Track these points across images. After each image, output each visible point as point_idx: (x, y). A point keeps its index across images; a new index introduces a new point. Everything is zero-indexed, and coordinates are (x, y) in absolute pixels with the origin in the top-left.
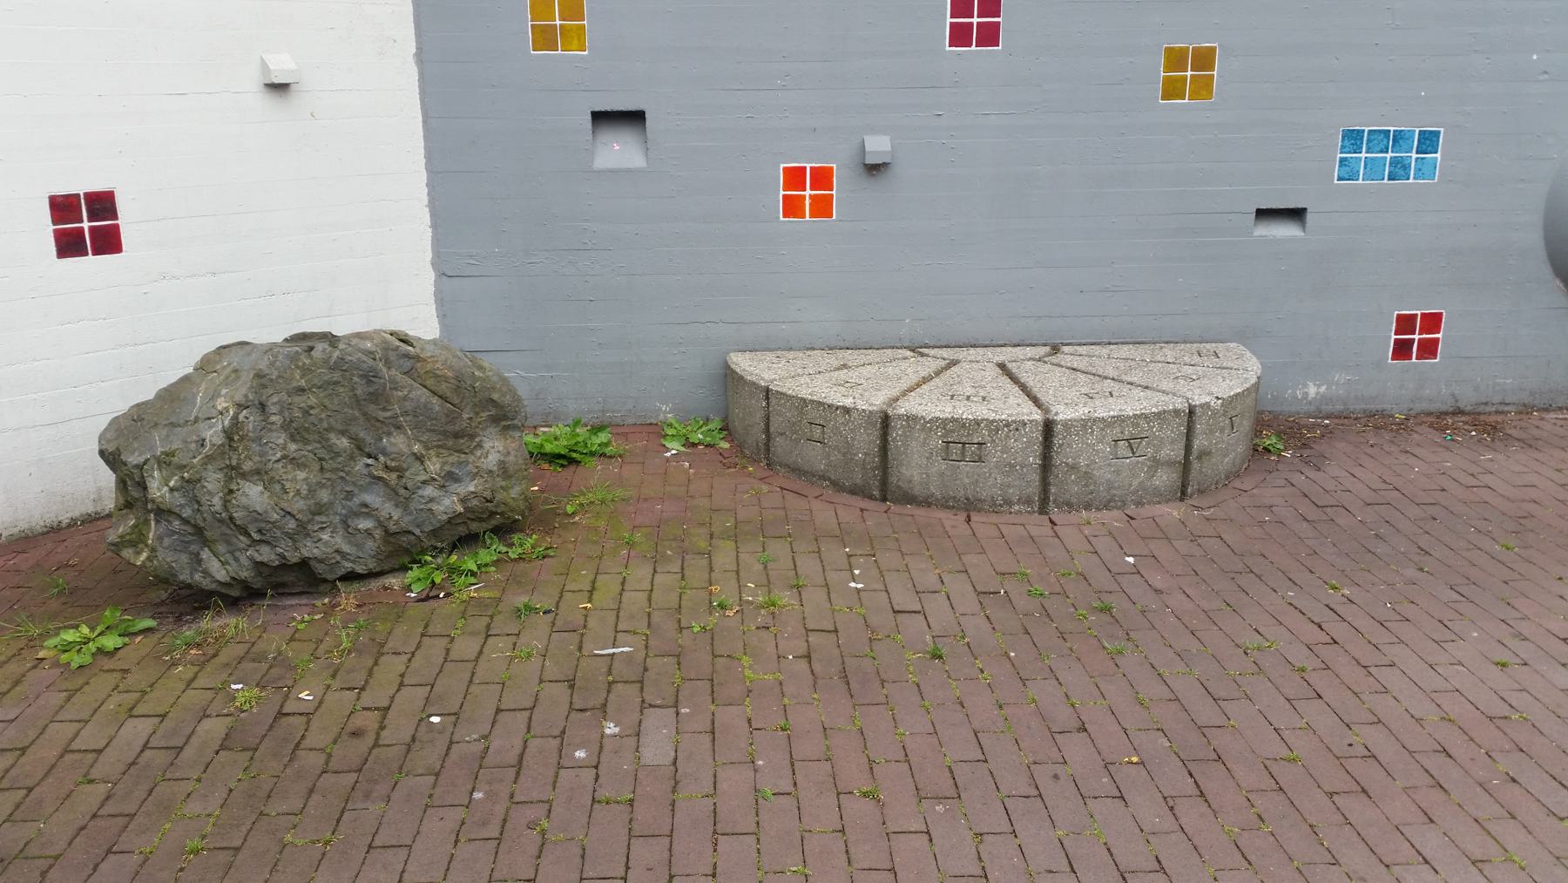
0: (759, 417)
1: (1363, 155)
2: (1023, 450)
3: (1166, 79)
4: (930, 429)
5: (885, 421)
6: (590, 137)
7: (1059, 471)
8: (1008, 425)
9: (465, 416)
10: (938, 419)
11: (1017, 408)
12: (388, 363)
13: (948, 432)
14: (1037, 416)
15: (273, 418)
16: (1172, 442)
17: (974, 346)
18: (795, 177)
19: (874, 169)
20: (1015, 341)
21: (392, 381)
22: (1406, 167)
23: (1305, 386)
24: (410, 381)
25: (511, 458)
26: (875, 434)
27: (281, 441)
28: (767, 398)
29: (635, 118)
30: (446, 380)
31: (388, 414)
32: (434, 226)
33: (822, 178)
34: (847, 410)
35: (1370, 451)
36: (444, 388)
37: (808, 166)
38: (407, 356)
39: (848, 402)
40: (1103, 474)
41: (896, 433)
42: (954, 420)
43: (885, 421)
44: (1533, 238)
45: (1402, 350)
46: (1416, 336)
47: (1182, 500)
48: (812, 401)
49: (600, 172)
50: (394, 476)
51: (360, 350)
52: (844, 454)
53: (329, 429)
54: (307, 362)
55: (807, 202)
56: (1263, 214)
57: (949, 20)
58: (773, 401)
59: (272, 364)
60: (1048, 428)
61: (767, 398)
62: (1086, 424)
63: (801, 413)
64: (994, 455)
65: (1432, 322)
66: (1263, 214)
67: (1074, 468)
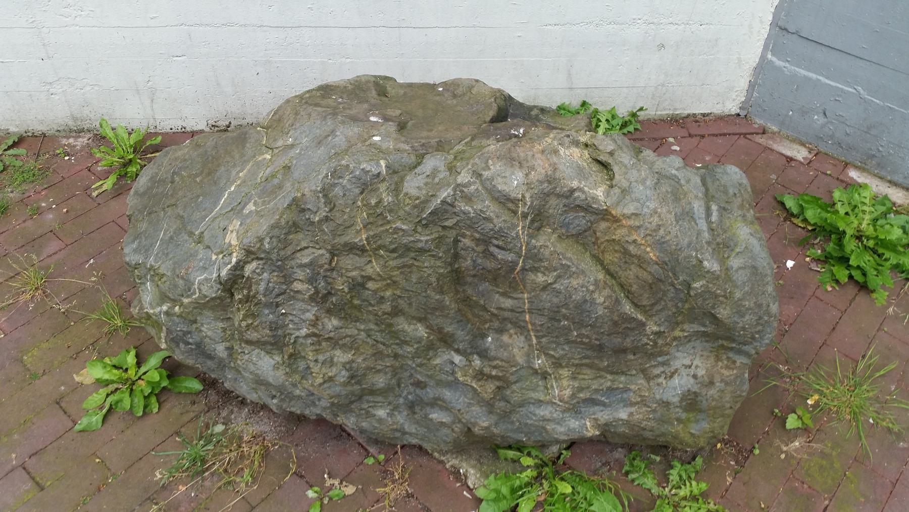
9: (652, 327)
15: (297, 286)
25: (712, 392)
27: (310, 316)
30: (641, 262)
31: (508, 303)
36: (631, 274)
50: (491, 387)
53: (396, 312)
54: (388, 199)
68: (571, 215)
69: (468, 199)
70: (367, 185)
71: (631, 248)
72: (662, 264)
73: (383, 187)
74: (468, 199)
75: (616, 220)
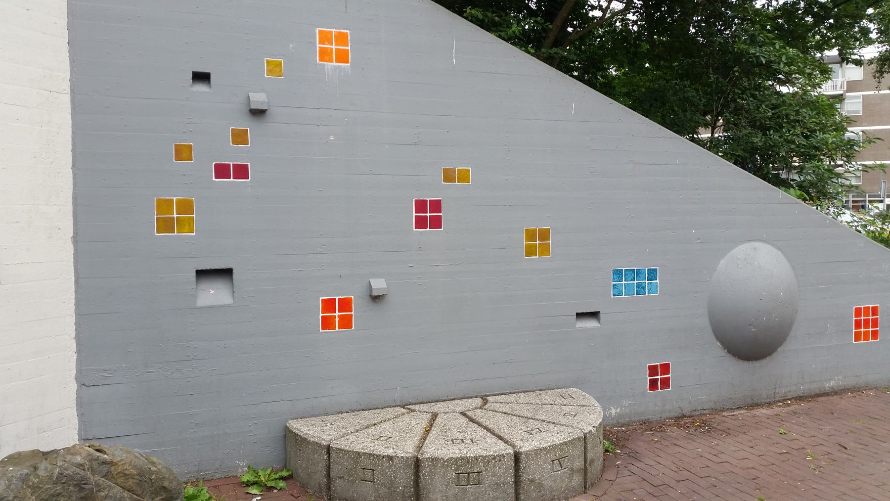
0: (321, 467)
1: (624, 282)
2: (504, 473)
3: (527, 246)
4: (447, 466)
5: (417, 463)
6: (194, 286)
7: (525, 485)
8: (494, 458)
10: (452, 458)
11: (491, 447)
12: (92, 470)
13: (459, 467)
14: (511, 451)
16: (579, 458)
17: (438, 401)
18: (329, 305)
19: (376, 299)
20: (460, 396)
21: (97, 485)
22: (644, 288)
23: (610, 409)
24: (109, 483)
26: (410, 472)
28: (328, 453)
29: (226, 273)
30: (132, 476)
32: (78, 352)
33: (345, 305)
34: (390, 458)
35: (656, 445)
36: (131, 483)
37: (337, 298)
38: (104, 463)
39: (390, 452)
40: (548, 483)
41: (425, 471)
42: (462, 458)
43: (417, 463)
44: (704, 321)
45: (653, 385)
46: (659, 377)
47: (585, 492)
48: (365, 454)
49: (201, 308)
51: (73, 464)
52: (389, 488)
54: (36, 481)
55: (337, 320)
56: (580, 315)
57: (414, 214)
58: (333, 455)
59: (8, 487)
60: (517, 457)
61: (328, 453)
62: (538, 452)
63: (356, 463)
64: (488, 479)
65: (665, 368)
66: (580, 315)
67: (532, 481)
68: (101, 468)
69: (66, 469)
70: (24, 479)
71: (126, 472)
72: (139, 475)
73: (31, 477)
74: (66, 469)
75: (116, 464)
